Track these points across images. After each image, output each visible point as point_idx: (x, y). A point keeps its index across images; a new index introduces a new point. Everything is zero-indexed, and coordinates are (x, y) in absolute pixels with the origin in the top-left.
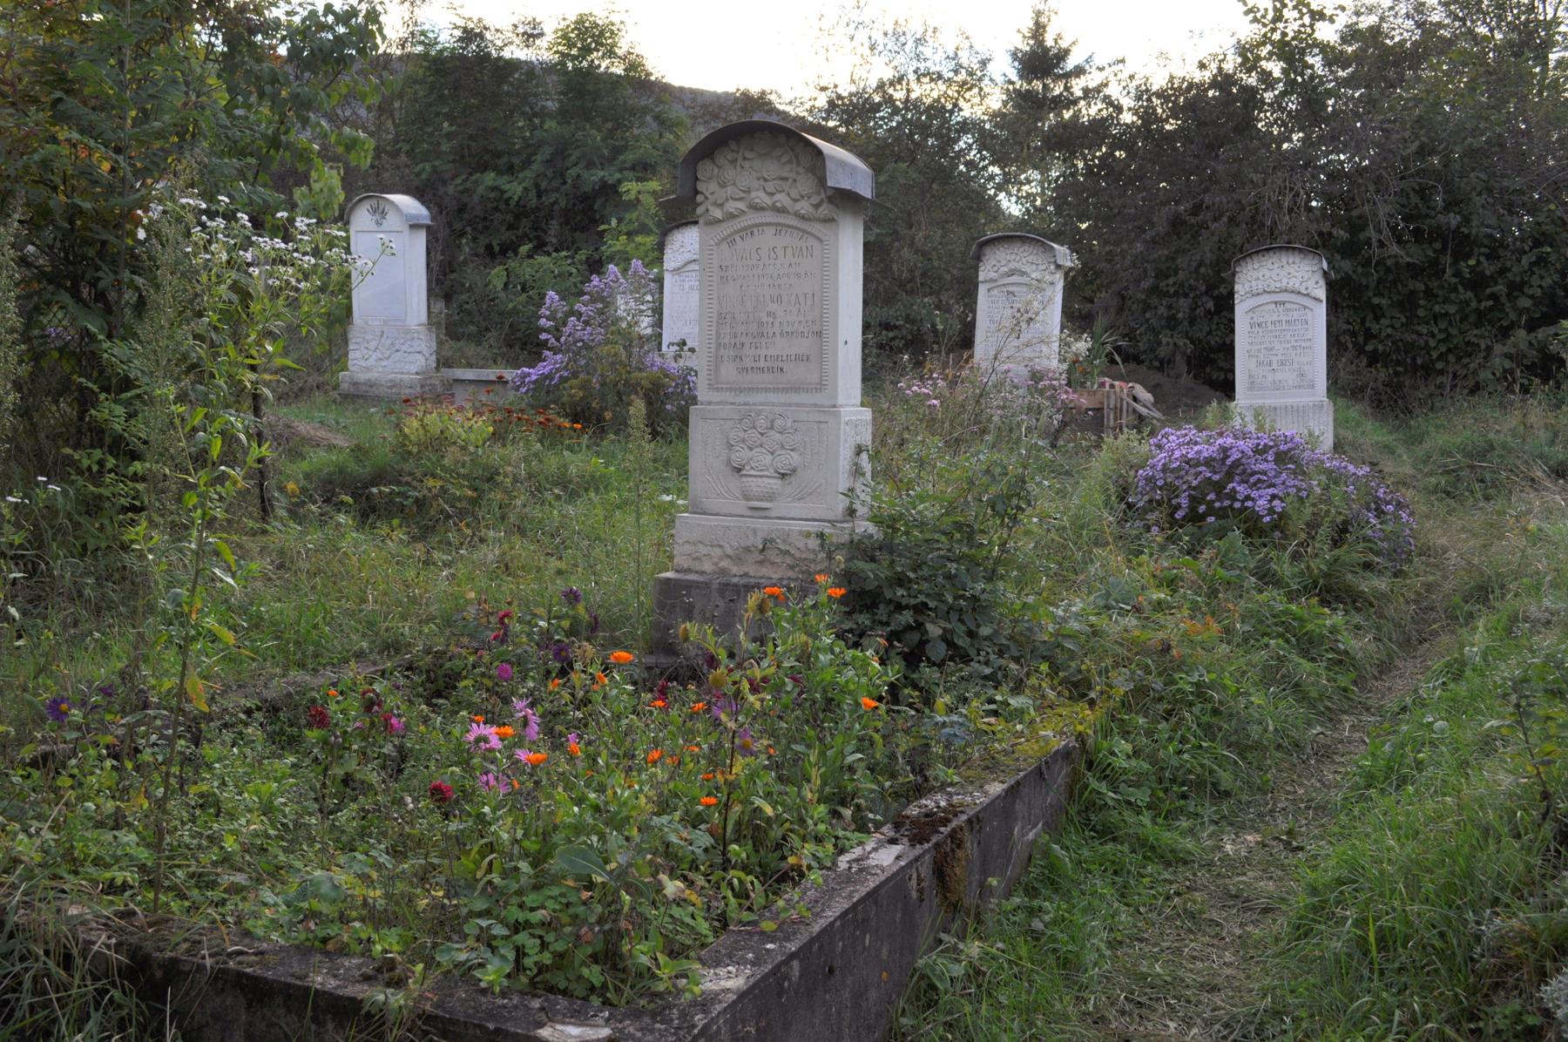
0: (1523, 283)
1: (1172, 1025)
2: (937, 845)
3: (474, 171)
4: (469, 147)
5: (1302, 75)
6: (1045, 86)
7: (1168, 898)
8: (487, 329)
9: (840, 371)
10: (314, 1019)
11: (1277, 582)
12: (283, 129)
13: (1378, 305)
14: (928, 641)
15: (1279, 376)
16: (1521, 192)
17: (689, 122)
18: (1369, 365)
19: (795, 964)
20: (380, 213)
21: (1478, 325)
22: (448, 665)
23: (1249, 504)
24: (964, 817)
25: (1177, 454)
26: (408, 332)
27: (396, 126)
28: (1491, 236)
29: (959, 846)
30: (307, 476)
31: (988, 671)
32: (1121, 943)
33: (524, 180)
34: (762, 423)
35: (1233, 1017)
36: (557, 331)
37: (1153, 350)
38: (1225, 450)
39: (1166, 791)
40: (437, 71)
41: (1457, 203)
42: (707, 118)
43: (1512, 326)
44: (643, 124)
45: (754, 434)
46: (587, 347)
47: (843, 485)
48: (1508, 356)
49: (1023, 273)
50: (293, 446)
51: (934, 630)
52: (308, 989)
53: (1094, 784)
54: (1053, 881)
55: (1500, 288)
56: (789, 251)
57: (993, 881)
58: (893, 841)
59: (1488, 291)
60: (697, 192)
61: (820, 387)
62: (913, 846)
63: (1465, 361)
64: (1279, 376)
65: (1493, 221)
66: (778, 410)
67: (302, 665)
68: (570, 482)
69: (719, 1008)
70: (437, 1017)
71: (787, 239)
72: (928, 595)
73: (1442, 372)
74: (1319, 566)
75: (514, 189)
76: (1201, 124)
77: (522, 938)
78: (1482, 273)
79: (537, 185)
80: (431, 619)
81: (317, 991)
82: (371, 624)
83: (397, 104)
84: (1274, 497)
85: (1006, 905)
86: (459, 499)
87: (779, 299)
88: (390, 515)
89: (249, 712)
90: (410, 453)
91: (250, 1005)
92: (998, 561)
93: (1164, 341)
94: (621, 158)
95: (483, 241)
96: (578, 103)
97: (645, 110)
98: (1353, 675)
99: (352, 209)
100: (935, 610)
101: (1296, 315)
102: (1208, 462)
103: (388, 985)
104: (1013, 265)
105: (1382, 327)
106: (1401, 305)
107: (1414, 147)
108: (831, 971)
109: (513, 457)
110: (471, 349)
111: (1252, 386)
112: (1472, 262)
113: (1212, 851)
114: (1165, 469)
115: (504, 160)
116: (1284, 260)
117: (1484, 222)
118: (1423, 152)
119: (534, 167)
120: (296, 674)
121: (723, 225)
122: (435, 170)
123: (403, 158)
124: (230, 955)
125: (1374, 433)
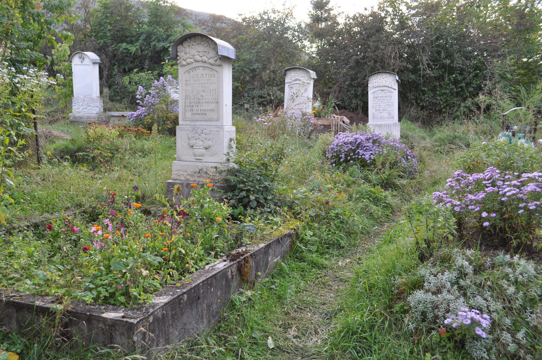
0: (471, 83)
1: (309, 314)
2: (238, 262)
3: (119, 43)
4: (117, 34)
5: (398, 13)
6: (322, 13)
7: (318, 279)
8: (124, 98)
9: (224, 115)
10: (36, 314)
11: (370, 182)
12: (42, 32)
13: (424, 90)
14: (251, 201)
15: (382, 114)
16: (470, 52)
17: (194, 26)
18: (421, 110)
19: (185, 295)
20: (82, 58)
21: (457, 96)
22: (97, 211)
23: (363, 156)
24: (249, 254)
25: (341, 141)
26: (93, 99)
27: (91, 27)
28: (460, 67)
29: (247, 263)
30: (55, 149)
31: (269, 210)
32: (299, 292)
33: (136, 46)
34: (199, 131)
35: (328, 312)
36: (142, 100)
37: (350, 105)
38: (356, 139)
39: (323, 246)
40: (105, 7)
41: (450, 56)
42: (201, 24)
43: (467, 97)
44: (178, 27)
45: (197, 135)
46: (153, 105)
47: (225, 151)
48: (465, 107)
49: (300, 80)
50: (50, 138)
51: (252, 197)
52: (34, 305)
53: (298, 244)
54: (281, 273)
55: (463, 84)
56: (207, 75)
57: (259, 273)
58: (225, 261)
59: (459, 85)
60: (177, 56)
61: (218, 120)
62: (230, 262)
63: (452, 109)
64: (382, 114)
65: (461, 62)
66: (204, 127)
67: (48, 212)
68: (145, 151)
69: (158, 307)
70: (72, 312)
71: (207, 71)
72: (251, 186)
73: (445, 112)
74: (384, 176)
75: (133, 49)
76: (365, 29)
77: (100, 289)
78: (457, 79)
79: (141, 48)
80: (92, 196)
81: (37, 306)
82: (72, 198)
83: (91, 19)
84: (371, 154)
85: (263, 279)
86: (106, 157)
87: (204, 91)
88: (83, 162)
89: (28, 227)
90: (90, 141)
91: (17, 311)
92: (274, 176)
93: (354, 102)
94: (170, 38)
95: (122, 67)
96: (155, 19)
97: (179, 22)
98: (390, 211)
99: (72, 57)
100: (253, 191)
101: (388, 94)
102: (351, 143)
103: (59, 304)
104: (296, 77)
105: (426, 97)
106: (432, 90)
107: (434, 37)
108: (199, 298)
109: (125, 143)
110: (118, 105)
111: (374, 118)
112: (454, 76)
113: (335, 264)
114: (337, 145)
115: (129, 39)
116: (384, 76)
117: (459, 62)
118: (438, 39)
119: (140, 41)
120: (46, 215)
121: (186, 67)
122: (105, 42)
123: (93, 38)
124: (11, 297)
125: (417, 131)
